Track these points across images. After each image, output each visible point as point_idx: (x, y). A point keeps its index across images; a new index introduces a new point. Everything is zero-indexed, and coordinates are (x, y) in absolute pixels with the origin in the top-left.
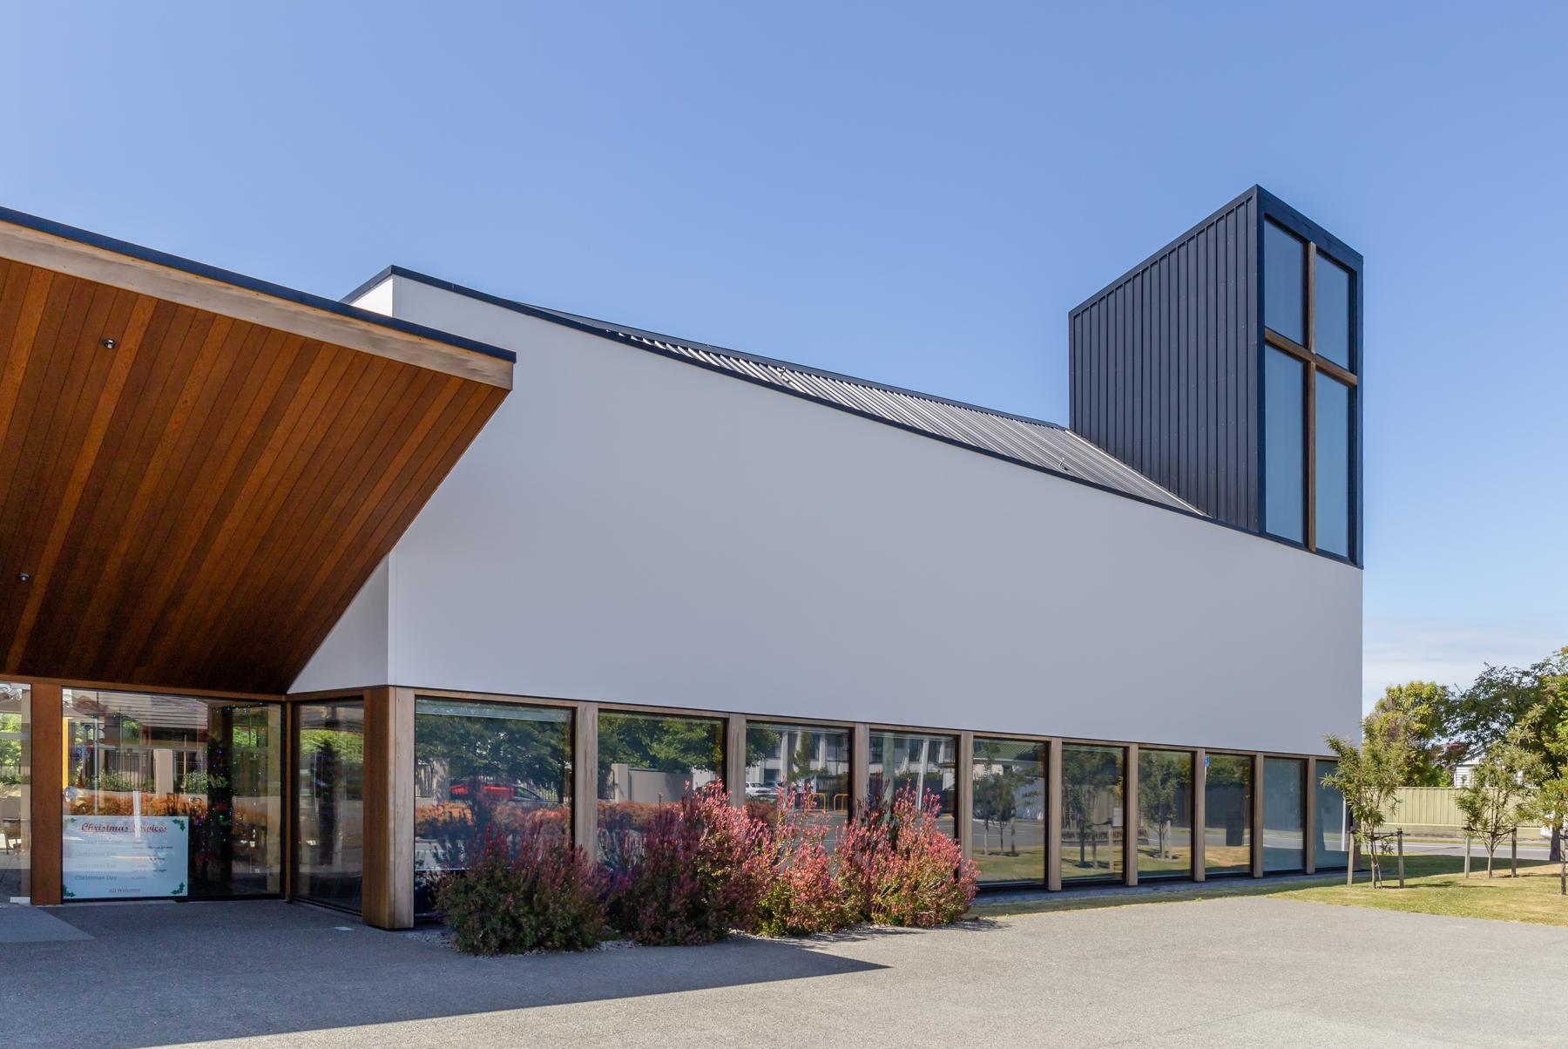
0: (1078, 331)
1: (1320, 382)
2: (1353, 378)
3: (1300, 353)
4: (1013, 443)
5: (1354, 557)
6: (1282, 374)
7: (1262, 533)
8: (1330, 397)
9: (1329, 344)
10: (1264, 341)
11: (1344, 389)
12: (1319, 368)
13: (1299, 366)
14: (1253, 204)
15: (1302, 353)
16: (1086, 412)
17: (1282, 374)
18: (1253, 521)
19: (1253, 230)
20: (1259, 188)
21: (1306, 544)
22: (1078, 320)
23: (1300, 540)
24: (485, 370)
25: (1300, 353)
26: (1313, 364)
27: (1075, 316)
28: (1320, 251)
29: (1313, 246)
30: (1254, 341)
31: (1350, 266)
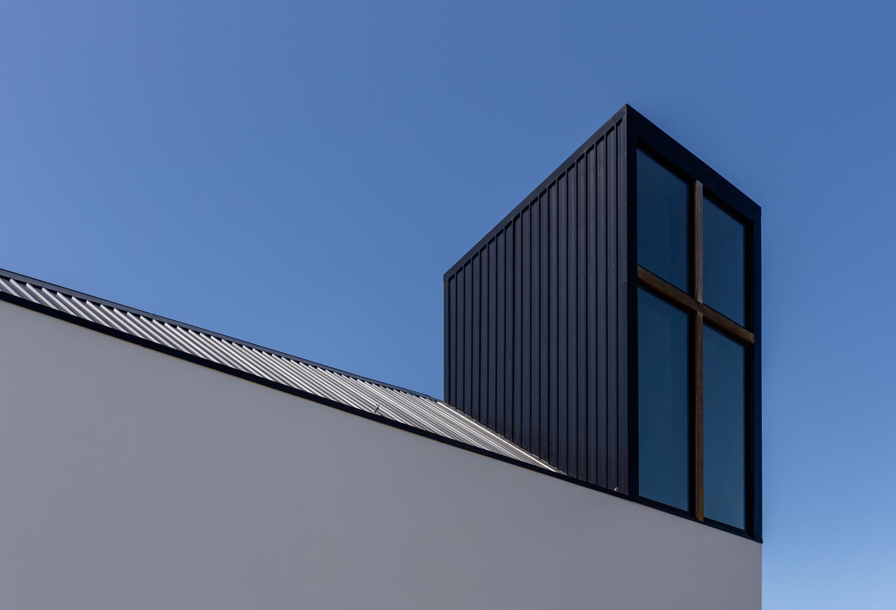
0: (453, 293)
1: (708, 339)
2: (750, 336)
3: (682, 302)
4: (140, 333)
5: (752, 529)
6: (661, 327)
7: (633, 495)
8: (720, 359)
9: (720, 294)
10: (635, 282)
11: (739, 351)
12: (707, 321)
13: (683, 318)
14: (623, 126)
15: (686, 300)
16: (602, 433)
17: (661, 327)
18: (624, 482)
19: (623, 155)
20: (628, 107)
21: (691, 514)
22: (453, 281)
23: (685, 508)
24: (723, 488)
25: (682, 302)
26: (700, 315)
27: (450, 278)
28: (707, 193)
29: (699, 185)
30: (624, 279)
31: (745, 213)
